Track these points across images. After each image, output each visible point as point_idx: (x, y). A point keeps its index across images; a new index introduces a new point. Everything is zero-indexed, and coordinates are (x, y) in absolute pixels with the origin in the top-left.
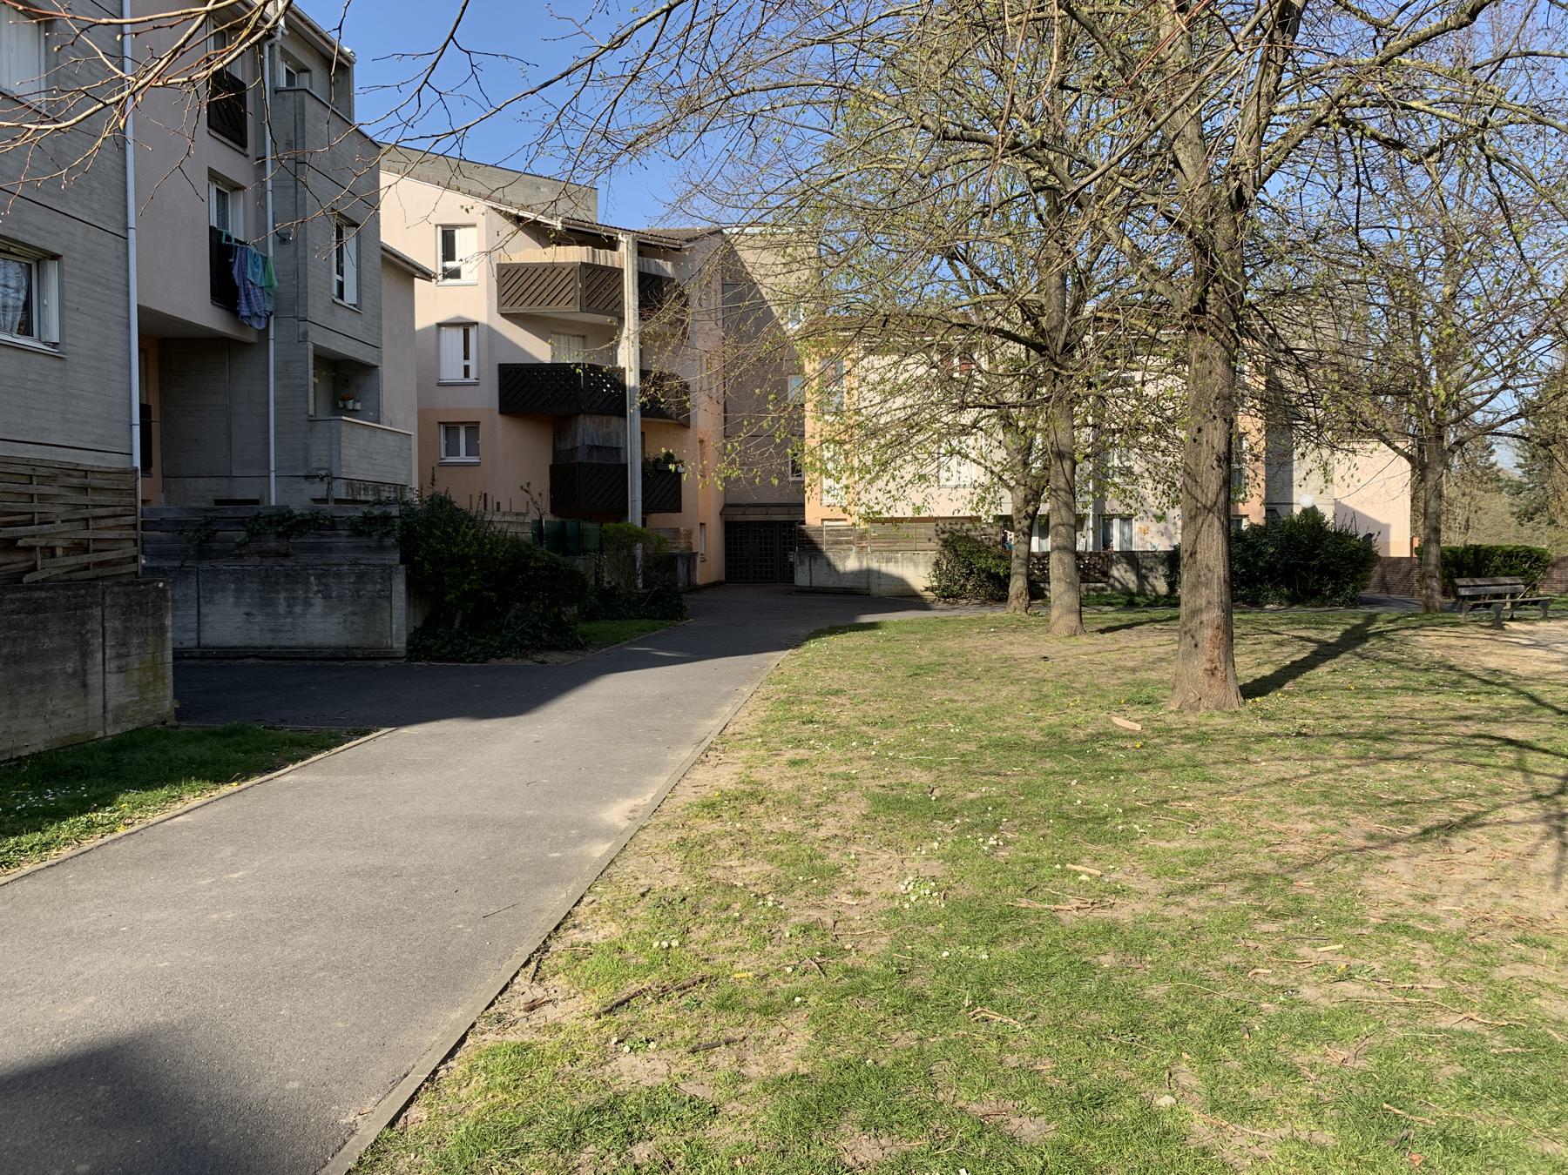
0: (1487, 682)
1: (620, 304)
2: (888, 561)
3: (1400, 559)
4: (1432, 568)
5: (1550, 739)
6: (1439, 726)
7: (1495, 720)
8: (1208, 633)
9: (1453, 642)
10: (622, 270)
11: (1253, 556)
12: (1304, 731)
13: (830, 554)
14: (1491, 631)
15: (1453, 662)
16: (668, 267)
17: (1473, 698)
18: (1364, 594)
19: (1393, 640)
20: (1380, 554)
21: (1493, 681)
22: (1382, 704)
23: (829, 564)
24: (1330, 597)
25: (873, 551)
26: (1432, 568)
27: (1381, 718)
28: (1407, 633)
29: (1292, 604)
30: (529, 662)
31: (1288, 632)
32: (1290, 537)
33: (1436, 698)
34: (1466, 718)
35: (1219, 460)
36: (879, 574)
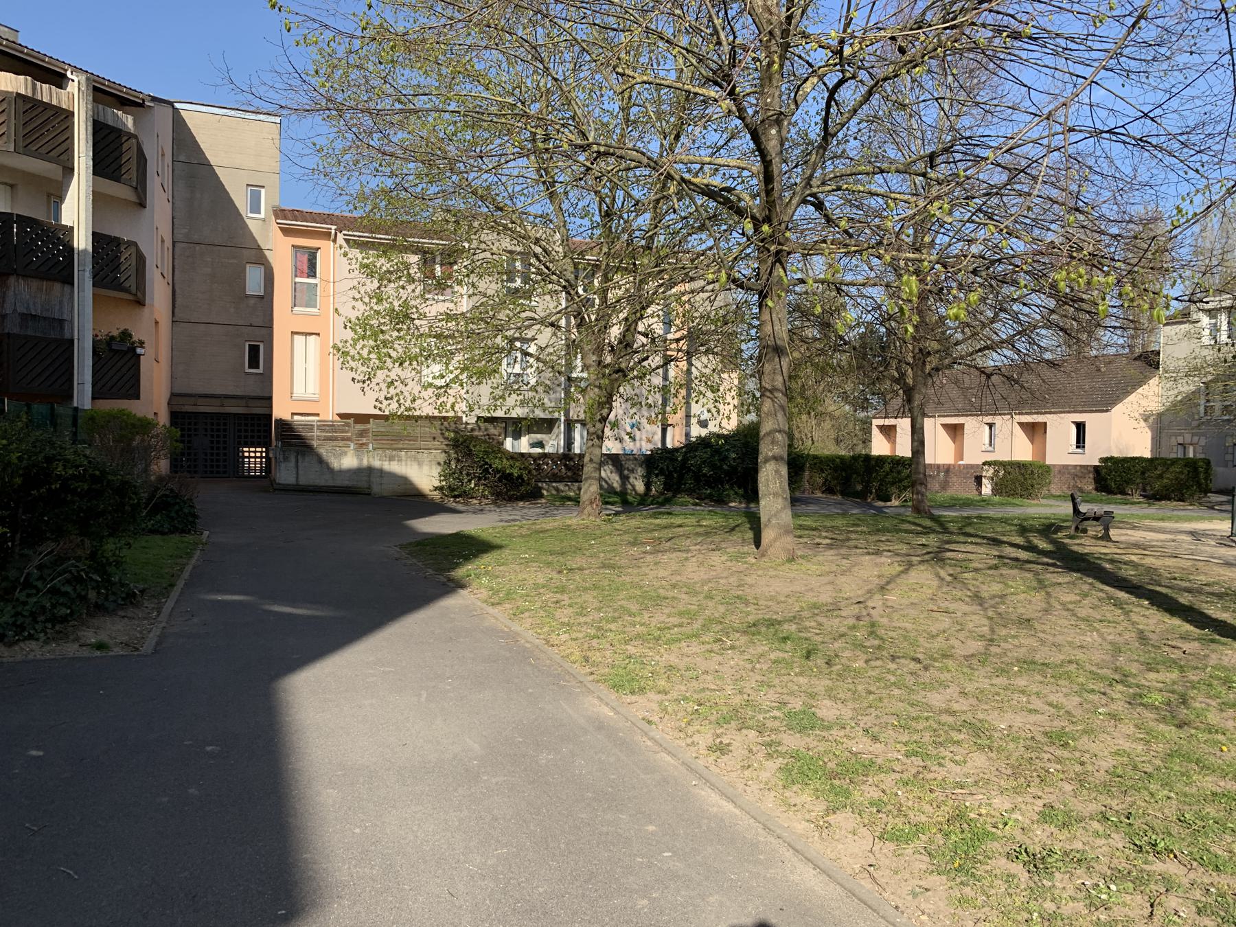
1: (70, 150)
2: (391, 459)
10: (72, 114)
11: (720, 460)
13: (322, 451)
16: (129, 122)
23: (321, 461)
25: (374, 449)
30: (71, 649)
36: (381, 472)
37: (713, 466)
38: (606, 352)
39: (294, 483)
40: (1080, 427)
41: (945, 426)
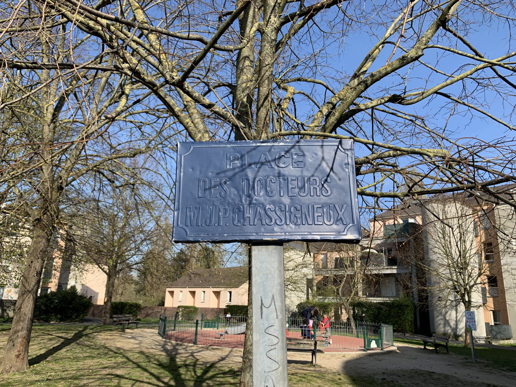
0: (116, 353)
3: (99, 305)
4: (107, 310)
5: (129, 374)
6: (97, 371)
7: (114, 368)
8: (20, 340)
9: (109, 337)
12: (50, 378)
14: (121, 333)
15: (107, 345)
17: (110, 359)
18: (86, 317)
19: (90, 337)
20: (94, 303)
21: (118, 352)
22: (80, 364)
24: (75, 319)
26: (107, 310)
27: (78, 370)
28: (95, 334)
29: (60, 322)
31: (55, 334)
32: (64, 297)
33: (98, 360)
34: (106, 368)
35: (37, 274)
37: (46, 305)
38: (64, 246)
39: (216, 307)
40: (230, 293)
41: (214, 292)
